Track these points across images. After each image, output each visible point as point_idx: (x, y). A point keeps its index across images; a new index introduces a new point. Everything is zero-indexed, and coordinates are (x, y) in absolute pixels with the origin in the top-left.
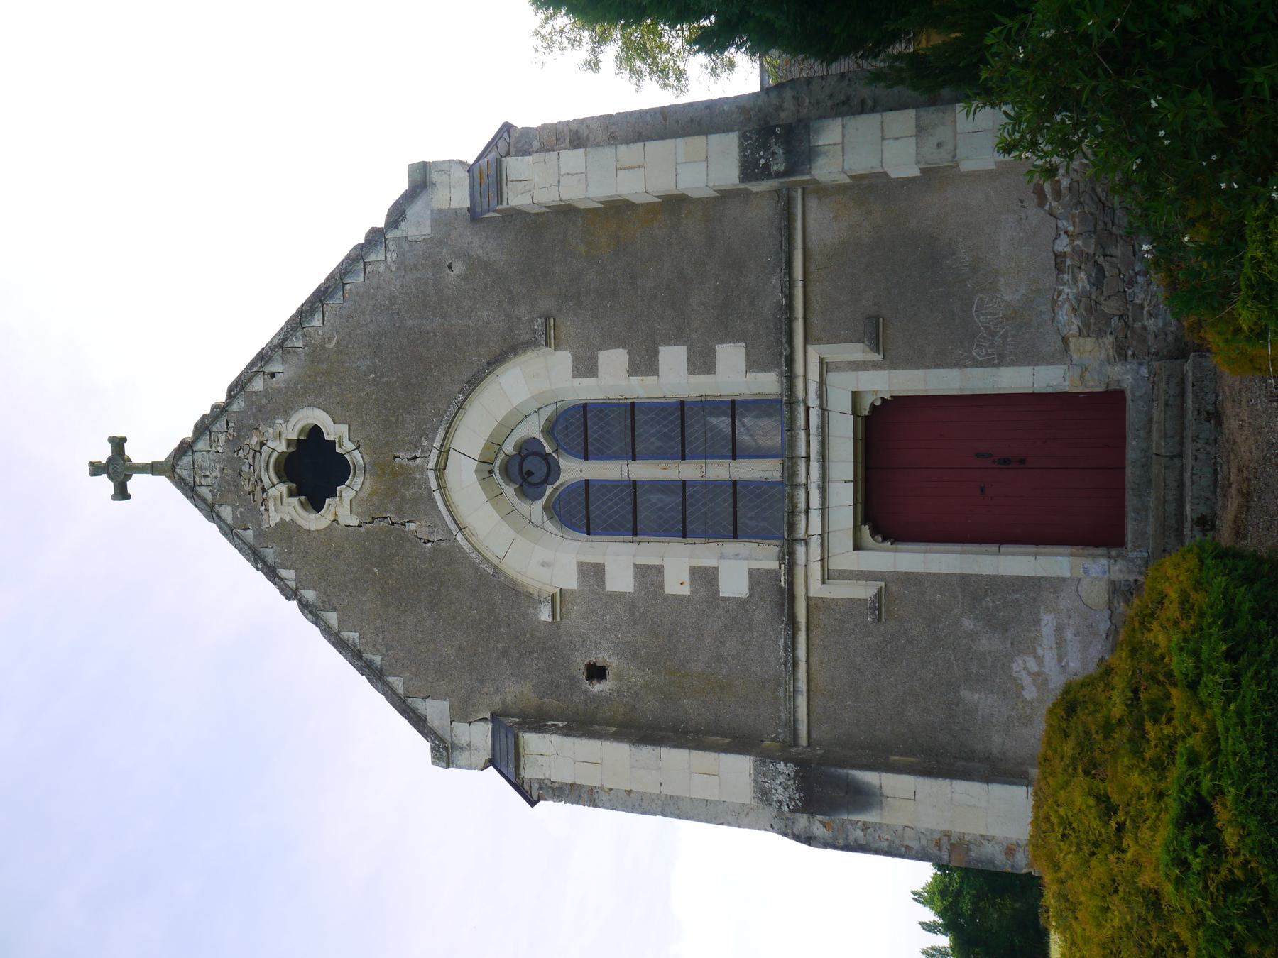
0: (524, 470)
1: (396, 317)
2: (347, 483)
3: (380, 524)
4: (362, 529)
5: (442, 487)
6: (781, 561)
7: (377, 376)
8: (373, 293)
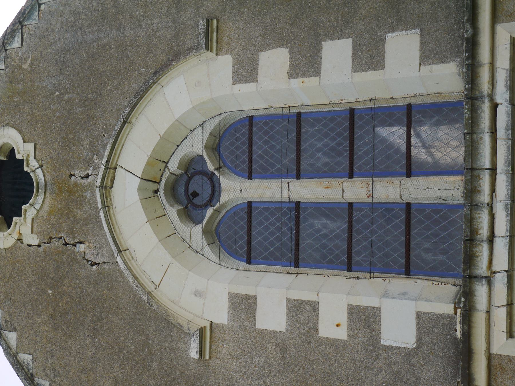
0: (190, 191)
1: (79, 33)
2: (31, 202)
3: (55, 244)
4: (41, 249)
5: (107, 206)
6: (456, 304)
7: (61, 94)
8: (62, 11)
